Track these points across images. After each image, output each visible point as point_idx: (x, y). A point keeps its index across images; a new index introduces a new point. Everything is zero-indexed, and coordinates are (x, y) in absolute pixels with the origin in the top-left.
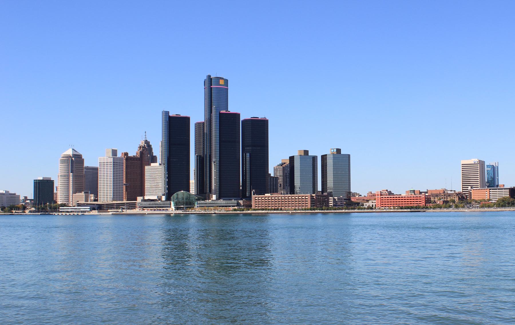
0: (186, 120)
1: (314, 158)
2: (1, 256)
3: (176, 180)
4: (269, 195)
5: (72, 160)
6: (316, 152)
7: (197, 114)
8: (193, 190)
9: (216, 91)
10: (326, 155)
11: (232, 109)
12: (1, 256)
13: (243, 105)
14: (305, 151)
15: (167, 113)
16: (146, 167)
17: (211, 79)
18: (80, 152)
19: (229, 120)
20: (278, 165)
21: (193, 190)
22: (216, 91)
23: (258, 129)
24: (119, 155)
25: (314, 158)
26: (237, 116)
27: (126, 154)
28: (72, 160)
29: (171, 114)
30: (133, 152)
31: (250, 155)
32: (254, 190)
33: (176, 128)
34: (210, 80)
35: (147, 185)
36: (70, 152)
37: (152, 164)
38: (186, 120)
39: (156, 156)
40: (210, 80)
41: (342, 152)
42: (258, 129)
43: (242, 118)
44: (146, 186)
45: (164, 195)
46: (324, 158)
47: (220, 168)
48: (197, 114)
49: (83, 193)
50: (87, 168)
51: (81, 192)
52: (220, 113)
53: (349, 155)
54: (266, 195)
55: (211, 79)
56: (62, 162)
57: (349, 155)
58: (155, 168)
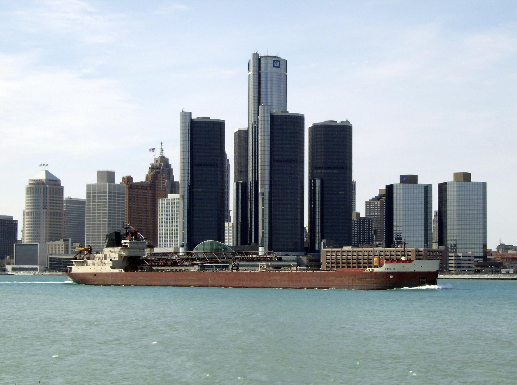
0: (218, 127)
1: (427, 189)
3: (203, 219)
4: (349, 248)
5: (45, 189)
7: (235, 114)
8: (230, 238)
9: (267, 75)
10: (393, 185)
11: (293, 108)
13: (310, 103)
15: (186, 115)
16: (161, 201)
19: (285, 128)
20: (373, 199)
21: (230, 238)
22: (267, 75)
23: (336, 140)
24: (118, 180)
25: (427, 189)
26: (299, 120)
27: (128, 179)
28: (45, 189)
29: (194, 117)
30: (140, 176)
31: (322, 183)
32: (324, 241)
33: (203, 135)
34: (258, 60)
35: (162, 229)
36: (42, 176)
37: (170, 196)
38: (218, 127)
39: (387, 186)
40: (258, 60)
41: (474, 179)
42: (336, 140)
43: (308, 124)
44: (159, 232)
45: (182, 246)
48: (235, 114)
49: (62, 241)
50: (70, 201)
51: (59, 240)
53: (484, 185)
54: (345, 248)
55: (259, 60)
56: (29, 191)
57: (484, 185)
58: (173, 202)
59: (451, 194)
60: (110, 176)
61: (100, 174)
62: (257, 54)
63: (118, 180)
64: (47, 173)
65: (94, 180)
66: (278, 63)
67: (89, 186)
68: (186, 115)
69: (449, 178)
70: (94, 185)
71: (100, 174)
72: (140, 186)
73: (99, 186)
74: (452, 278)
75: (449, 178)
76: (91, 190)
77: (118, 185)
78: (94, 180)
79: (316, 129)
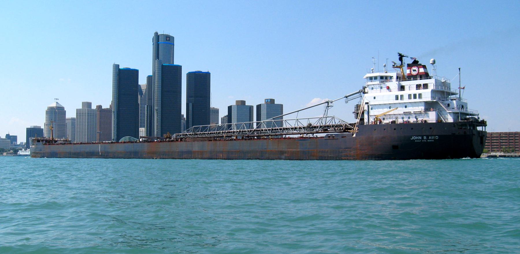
2: (518, 247)
6: (252, 101)
9: (163, 45)
12: (518, 247)
14: (271, 100)
15: (116, 67)
17: (158, 36)
18: (62, 104)
22: (163, 45)
23: (201, 82)
24: (94, 107)
25: (251, 108)
26: (179, 68)
27: (99, 107)
28: (55, 112)
29: (121, 67)
33: (125, 79)
34: (157, 36)
36: (54, 105)
38: (134, 74)
40: (157, 36)
46: (259, 107)
47: (162, 122)
52: (163, 66)
53: (282, 105)
56: (47, 112)
57: (282, 105)
59: (264, 112)
60: (89, 105)
61: (84, 104)
62: (156, 34)
63: (94, 107)
64: (57, 103)
65: (80, 107)
66: (169, 40)
67: (78, 110)
68: (116, 67)
69: (262, 102)
70: (80, 109)
71: (84, 104)
72: (106, 110)
73: (82, 109)
74: (509, 157)
75: (262, 102)
76: (78, 112)
77: (93, 110)
78: (80, 107)
79: (190, 75)
